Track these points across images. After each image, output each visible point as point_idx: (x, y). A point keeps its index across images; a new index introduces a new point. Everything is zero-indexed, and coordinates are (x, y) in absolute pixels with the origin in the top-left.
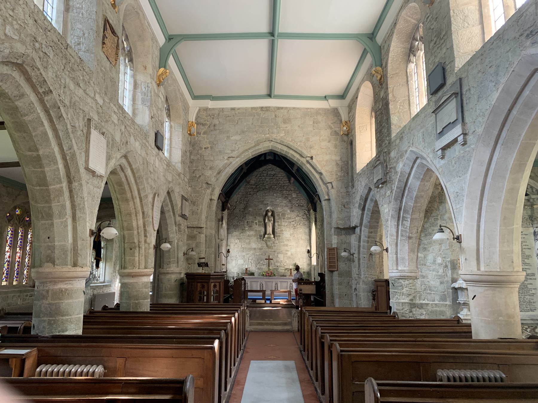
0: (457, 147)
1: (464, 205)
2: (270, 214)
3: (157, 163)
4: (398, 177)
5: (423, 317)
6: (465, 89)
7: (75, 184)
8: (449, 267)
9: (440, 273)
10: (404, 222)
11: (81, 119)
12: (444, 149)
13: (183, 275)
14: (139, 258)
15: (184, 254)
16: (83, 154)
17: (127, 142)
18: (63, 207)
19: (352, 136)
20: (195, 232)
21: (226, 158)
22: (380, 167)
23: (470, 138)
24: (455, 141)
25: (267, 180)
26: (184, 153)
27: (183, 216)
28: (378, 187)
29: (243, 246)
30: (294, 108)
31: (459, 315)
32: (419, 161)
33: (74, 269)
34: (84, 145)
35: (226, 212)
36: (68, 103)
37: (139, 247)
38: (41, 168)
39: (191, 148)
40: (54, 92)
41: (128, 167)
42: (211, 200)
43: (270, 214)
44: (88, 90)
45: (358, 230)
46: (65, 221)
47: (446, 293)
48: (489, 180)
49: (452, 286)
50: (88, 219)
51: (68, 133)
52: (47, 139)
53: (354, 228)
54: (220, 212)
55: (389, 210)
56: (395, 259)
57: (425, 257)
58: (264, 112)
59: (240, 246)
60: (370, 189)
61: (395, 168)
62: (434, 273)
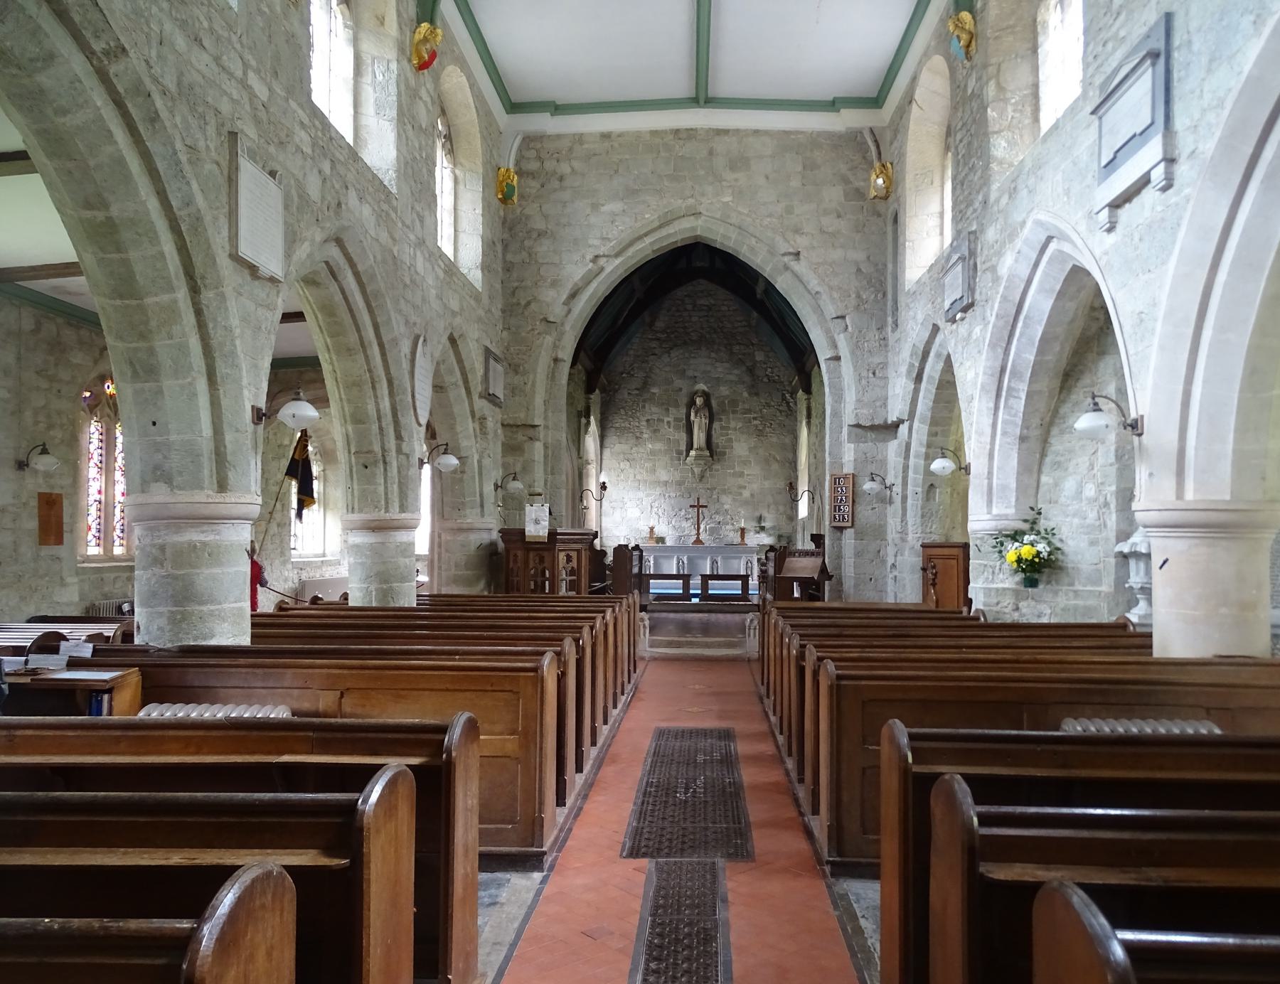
0: (1149, 196)
1: (1156, 341)
2: (699, 401)
3: (420, 264)
4: (1001, 290)
5: (1045, 620)
6: (1176, 41)
7: (207, 296)
8: (1113, 506)
9: (1088, 521)
10: (1012, 401)
11: (211, 130)
12: (1116, 205)
13: (495, 536)
14: (386, 488)
15: (496, 487)
16: (223, 222)
17: (339, 204)
18: (183, 349)
19: (898, 200)
20: (520, 437)
21: (589, 257)
22: (959, 268)
23: (1183, 170)
24: (1145, 181)
25: (694, 319)
26: (488, 246)
27: (491, 398)
28: (953, 321)
29: (638, 477)
30: (756, 132)
31: (1128, 615)
32: (1053, 246)
33: (219, 498)
34: (224, 199)
35: (596, 397)
36: (172, 87)
37: (385, 463)
38: (119, 250)
39: (506, 236)
40: (132, 54)
41: (347, 267)
42: (556, 360)
43: (699, 401)
44: (225, 58)
45: (903, 429)
46: (190, 384)
47: (1101, 566)
48: (1222, 276)
49: (1117, 549)
50: (245, 382)
51: (178, 163)
52: (127, 178)
53: (896, 425)
54: (580, 395)
55: (977, 374)
56: (985, 489)
57: (1056, 485)
58: (681, 142)
59: (632, 476)
60: (936, 329)
61: (993, 269)
62: (1076, 521)
